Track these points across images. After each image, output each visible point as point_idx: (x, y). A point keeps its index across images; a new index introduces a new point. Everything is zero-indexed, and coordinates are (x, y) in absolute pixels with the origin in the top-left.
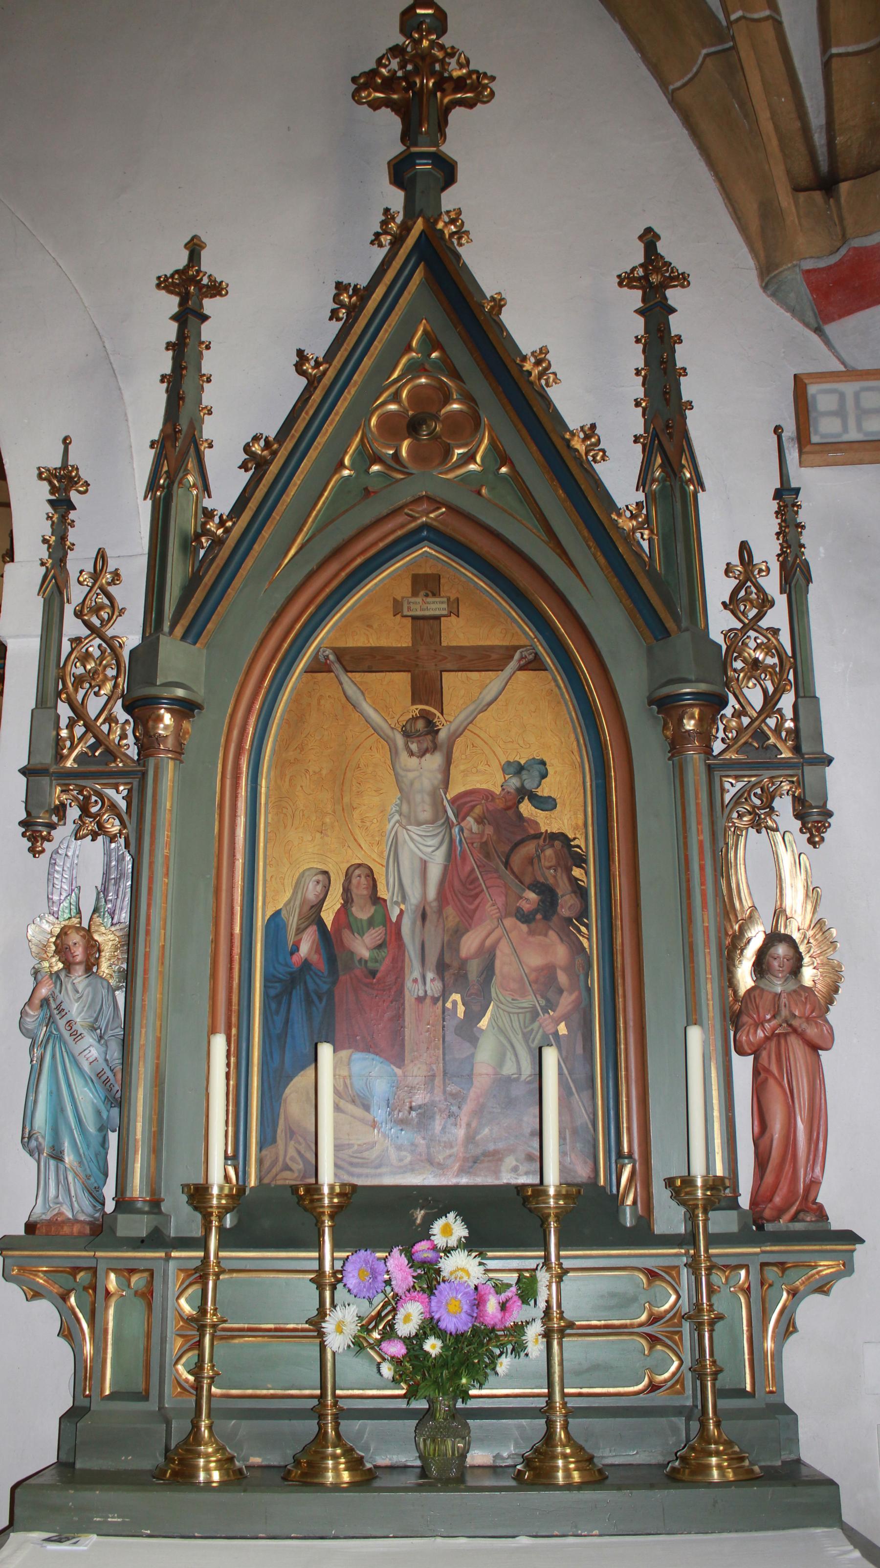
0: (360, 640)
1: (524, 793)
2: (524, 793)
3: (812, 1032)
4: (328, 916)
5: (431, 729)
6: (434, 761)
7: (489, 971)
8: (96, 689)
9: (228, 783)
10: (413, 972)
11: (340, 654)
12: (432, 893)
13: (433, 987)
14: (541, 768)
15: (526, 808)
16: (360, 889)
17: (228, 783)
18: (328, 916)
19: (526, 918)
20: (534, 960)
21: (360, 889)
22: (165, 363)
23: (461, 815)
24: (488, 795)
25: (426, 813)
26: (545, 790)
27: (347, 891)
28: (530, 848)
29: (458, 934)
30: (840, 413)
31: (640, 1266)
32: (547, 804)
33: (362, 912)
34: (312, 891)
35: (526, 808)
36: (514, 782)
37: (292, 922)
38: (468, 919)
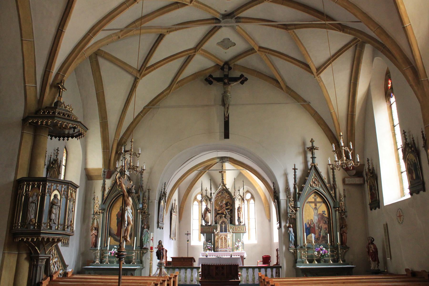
0: (310, 201)
1: (324, 213)
2: (324, 213)
3: (346, 232)
4: (309, 223)
5: (316, 208)
6: (317, 211)
7: (322, 227)
8: (340, 211)
9: (107, 222)
10: (316, 227)
11: (309, 202)
12: (317, 221)
13: (318, 229)
14: (325, 211)
15: (324, 215)
16: (312, 221)
17: (107, 222)
18: (309, 223)
19: (324, 223)
20: (325, 227)
21: (312, 221)
22: (294, 177)
23: (319, 215)
24: (321, 214)
25: (316, 215)
26: (325, 213)
27: (311, 221)
28: (324, 218)
29: (319, 225)
30: (348, 181)
31: (334, 213)
32: (325, 214)
33: (312, 223)
34: (308, 221)
35: (324, 215)
36: (323, 213)
37: (307, 224)
38: (320, 223)
